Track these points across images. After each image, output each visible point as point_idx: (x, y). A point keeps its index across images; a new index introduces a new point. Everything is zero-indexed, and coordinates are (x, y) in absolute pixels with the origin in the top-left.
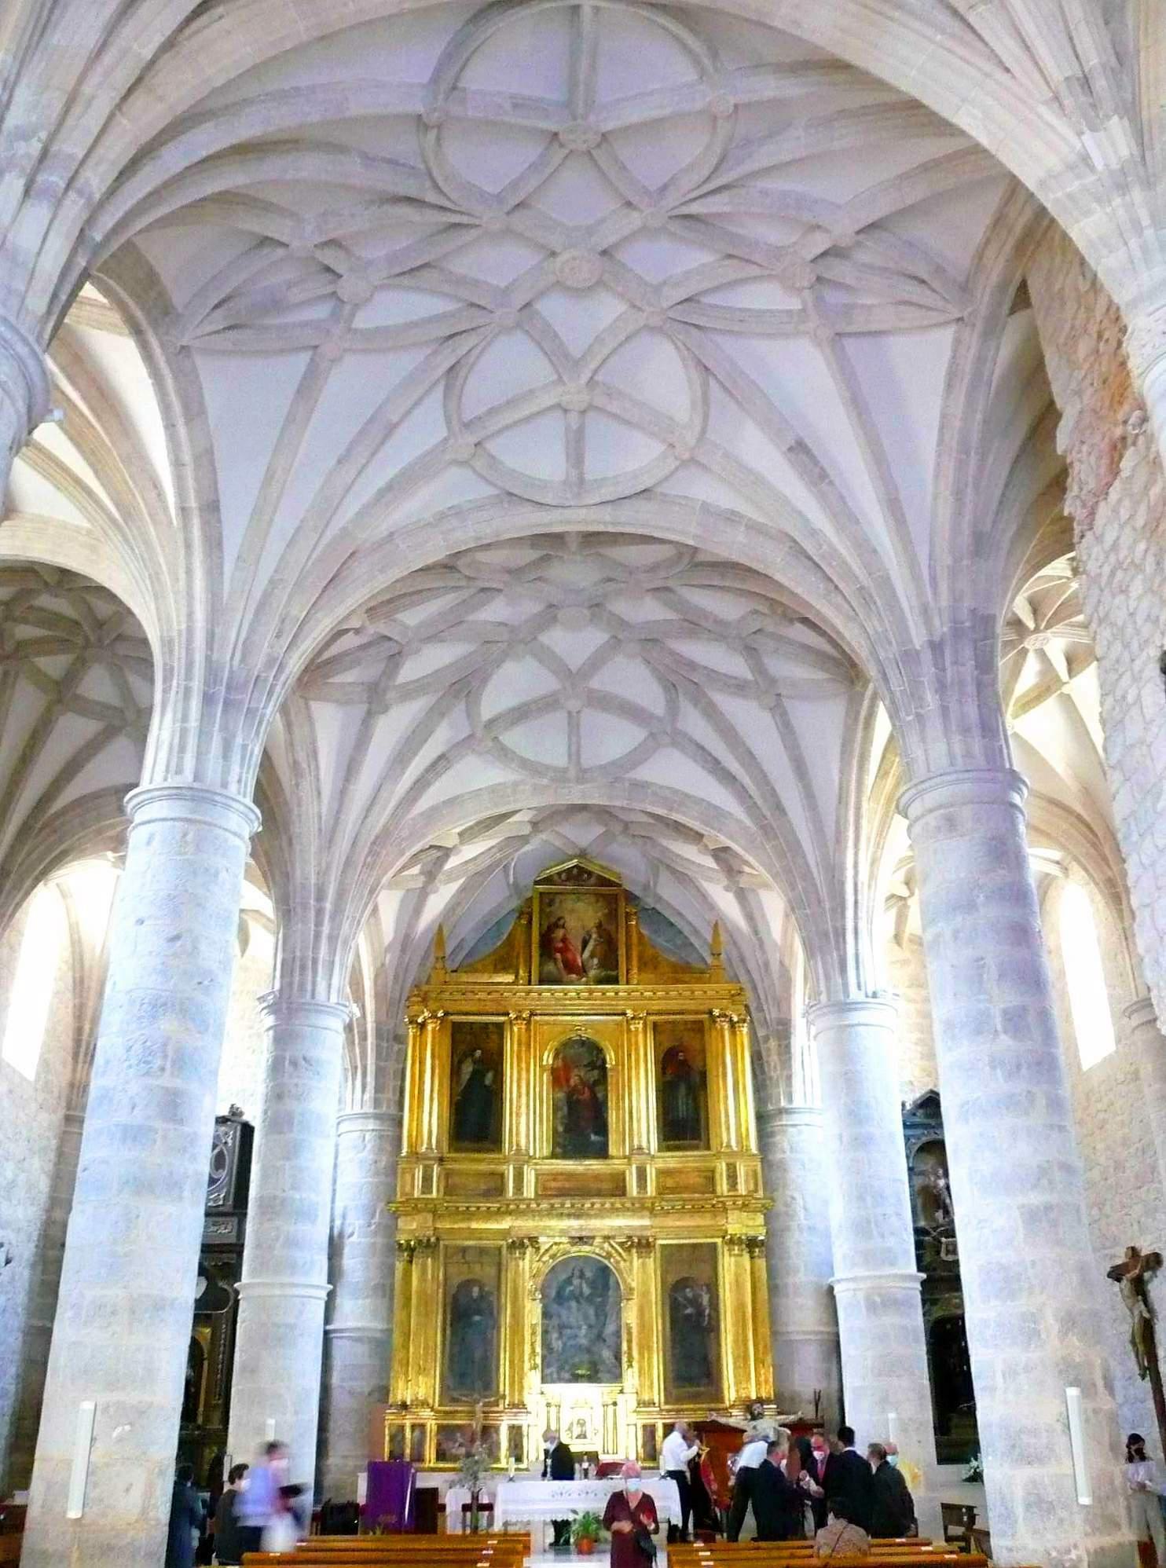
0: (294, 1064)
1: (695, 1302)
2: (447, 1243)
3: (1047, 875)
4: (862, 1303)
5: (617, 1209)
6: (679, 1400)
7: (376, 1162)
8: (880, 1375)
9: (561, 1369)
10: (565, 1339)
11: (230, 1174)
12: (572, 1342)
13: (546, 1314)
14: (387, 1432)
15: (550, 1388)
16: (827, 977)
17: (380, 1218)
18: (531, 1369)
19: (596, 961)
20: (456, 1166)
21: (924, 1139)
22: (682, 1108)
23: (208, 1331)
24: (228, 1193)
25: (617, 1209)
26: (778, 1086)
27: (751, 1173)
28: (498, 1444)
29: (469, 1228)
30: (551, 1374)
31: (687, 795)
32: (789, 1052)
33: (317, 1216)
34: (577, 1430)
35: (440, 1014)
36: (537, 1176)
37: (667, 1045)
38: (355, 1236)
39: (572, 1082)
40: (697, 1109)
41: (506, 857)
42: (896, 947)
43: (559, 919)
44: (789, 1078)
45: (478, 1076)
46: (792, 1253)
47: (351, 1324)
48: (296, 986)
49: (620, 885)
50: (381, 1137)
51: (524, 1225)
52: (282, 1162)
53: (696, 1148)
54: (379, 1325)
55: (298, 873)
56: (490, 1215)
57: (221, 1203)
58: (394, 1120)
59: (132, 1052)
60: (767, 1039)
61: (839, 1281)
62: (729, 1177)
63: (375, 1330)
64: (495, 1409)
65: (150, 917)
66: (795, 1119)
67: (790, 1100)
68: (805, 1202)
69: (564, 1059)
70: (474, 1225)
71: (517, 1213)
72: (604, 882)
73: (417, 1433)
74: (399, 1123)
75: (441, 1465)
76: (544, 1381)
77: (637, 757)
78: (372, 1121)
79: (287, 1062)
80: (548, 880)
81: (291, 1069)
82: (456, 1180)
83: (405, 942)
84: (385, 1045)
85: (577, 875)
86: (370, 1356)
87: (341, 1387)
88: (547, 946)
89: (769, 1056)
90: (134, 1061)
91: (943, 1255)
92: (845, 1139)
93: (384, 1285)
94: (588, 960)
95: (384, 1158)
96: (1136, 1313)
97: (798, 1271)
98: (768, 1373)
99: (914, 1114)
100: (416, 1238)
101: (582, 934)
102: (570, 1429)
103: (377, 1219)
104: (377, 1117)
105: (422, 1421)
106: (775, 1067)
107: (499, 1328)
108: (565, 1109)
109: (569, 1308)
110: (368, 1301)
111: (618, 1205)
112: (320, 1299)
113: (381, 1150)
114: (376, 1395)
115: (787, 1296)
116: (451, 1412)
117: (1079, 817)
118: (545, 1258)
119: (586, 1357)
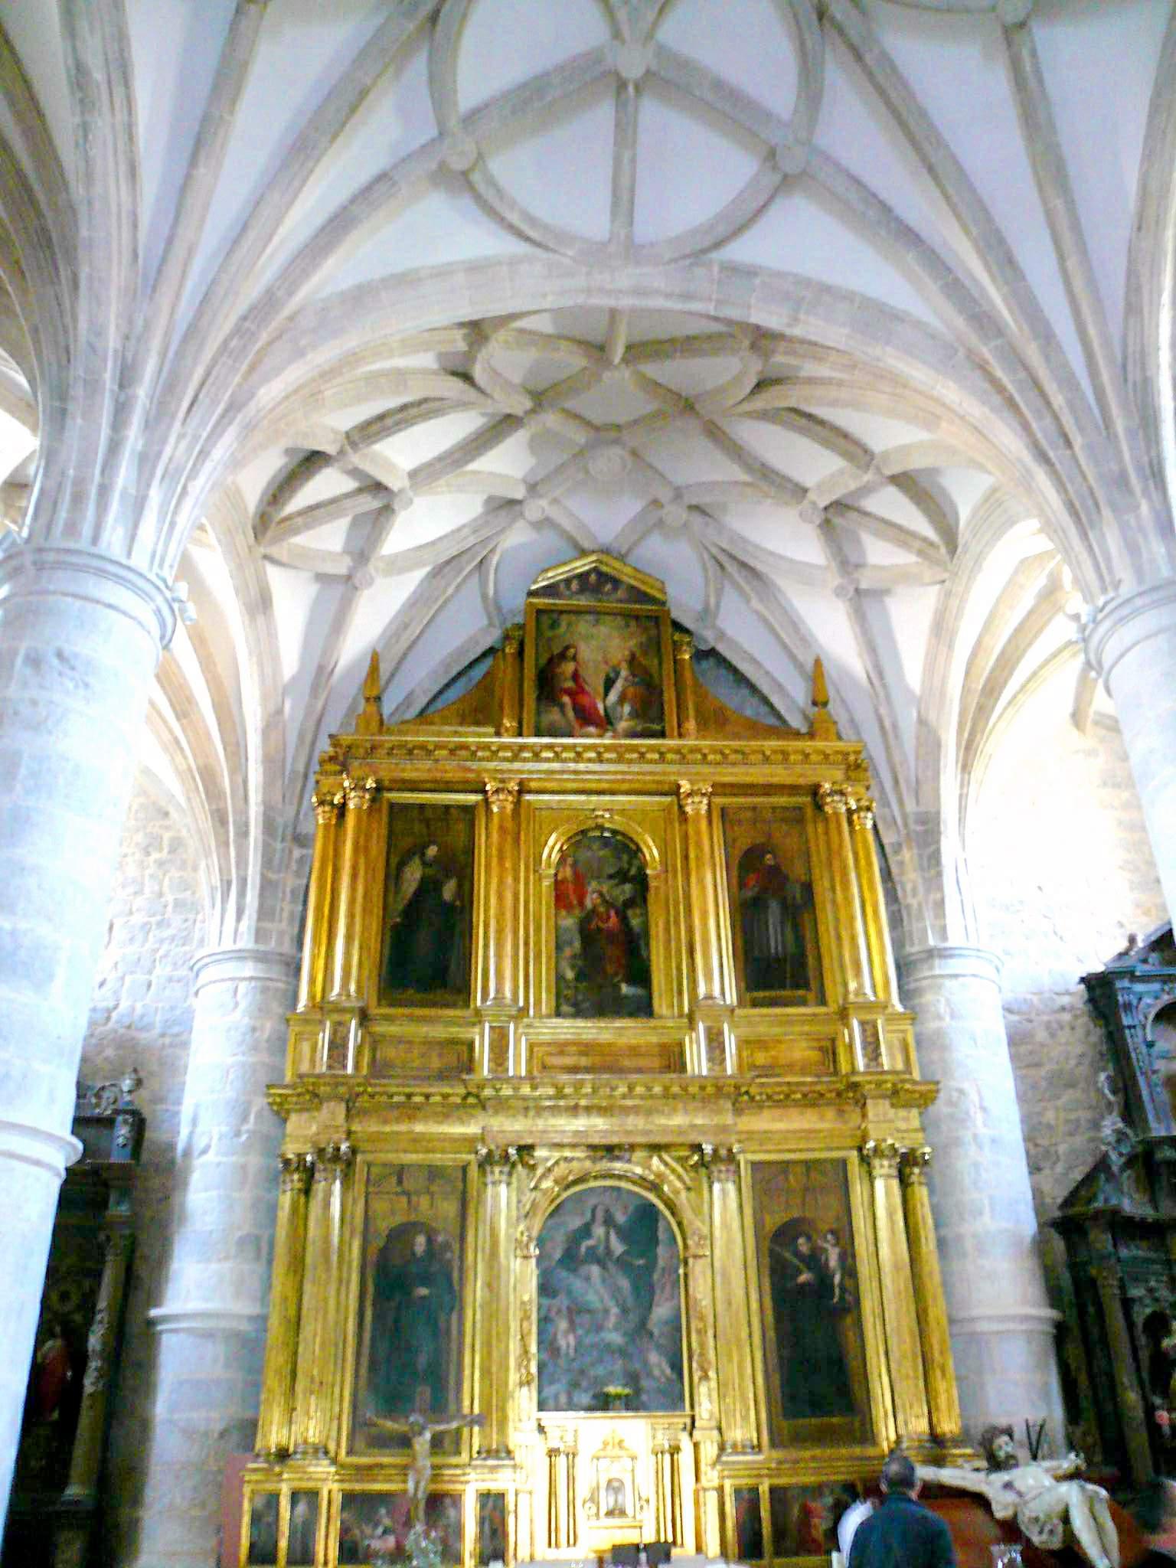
0: (35, 661)
1: (814, 1262)
2: (370, 1157)
5: (675, 1097)
6: (797, 1439)
7: (254, 1029)
9: (575, 1385)
10: (580, 1332)
12: (591, 1339)
13: (546, 1289)
14: (246, 1506)
15: (549, 1418)
17: (256, 1123)
18: (521, 1384)
20: (393, 1029)
22: (776, 937)
25: (675, 1097)
26: (920, 917)
27: (896, 1043)
28: (459, 1531)
29: (411, 1132)
30: (556, 1397)
31: (827, 289)
32: (938, 863)
33: (51, 977)
34: (606, 1501)
35: (370, 784)
36: (531, 1048)
37: (744, 843)
39: (589, 904)
40: (800, 939)
41: (484, 542)
42: (1075, 731)
43: (567, 648)
44: (940, 904)
45: (429, 887)
46: (967, 1181)
47: (193, 1305)
49: (663, 603)
50: (265, 990)
51: (510, 1127)
53: (803, 1003)
54: (248, 1308)
55: (83, 324)
56: (448, 1111)
58: (288, 964)
60: (898, 848)
62: (865, 1045)
63: (239, 1317)
64: (454, 1460)
68: (981, 1099)
69: (574, 865)
70: (419, 1128)
71: (501, 1105)
72: (639, 595)
73: (301, 1508)
74: (294, 968)
76: (541, 1407)
79: (19, 661)
80: (550, 590)
82: (389, 1052)
83: (321, 674)
84: (279, 846)
85: (596, 582)
86: (227, 1366)
87: (170, 1422)
88: (547, 687)
89: (902, 874)
93: (258, 1238)
95: (268, 1025)
97: (981, 1214)
99: (1145, 961)
100: (314, 1144)
101: (603, 670)
102: (594, 1499)
103: (250, 1125)
105: (311, 1485)
107: (462, 1309)
108: (577, 944)
109: (587, 1279)
110: (228, 1265)
111: (675, 1089)
112: (48, 1167)
113: (262, 1010)
114: (235, 1437)
115: (964, 1255)
116: (370, 1467)
118: (547, 1184)
119: (618, 1365)
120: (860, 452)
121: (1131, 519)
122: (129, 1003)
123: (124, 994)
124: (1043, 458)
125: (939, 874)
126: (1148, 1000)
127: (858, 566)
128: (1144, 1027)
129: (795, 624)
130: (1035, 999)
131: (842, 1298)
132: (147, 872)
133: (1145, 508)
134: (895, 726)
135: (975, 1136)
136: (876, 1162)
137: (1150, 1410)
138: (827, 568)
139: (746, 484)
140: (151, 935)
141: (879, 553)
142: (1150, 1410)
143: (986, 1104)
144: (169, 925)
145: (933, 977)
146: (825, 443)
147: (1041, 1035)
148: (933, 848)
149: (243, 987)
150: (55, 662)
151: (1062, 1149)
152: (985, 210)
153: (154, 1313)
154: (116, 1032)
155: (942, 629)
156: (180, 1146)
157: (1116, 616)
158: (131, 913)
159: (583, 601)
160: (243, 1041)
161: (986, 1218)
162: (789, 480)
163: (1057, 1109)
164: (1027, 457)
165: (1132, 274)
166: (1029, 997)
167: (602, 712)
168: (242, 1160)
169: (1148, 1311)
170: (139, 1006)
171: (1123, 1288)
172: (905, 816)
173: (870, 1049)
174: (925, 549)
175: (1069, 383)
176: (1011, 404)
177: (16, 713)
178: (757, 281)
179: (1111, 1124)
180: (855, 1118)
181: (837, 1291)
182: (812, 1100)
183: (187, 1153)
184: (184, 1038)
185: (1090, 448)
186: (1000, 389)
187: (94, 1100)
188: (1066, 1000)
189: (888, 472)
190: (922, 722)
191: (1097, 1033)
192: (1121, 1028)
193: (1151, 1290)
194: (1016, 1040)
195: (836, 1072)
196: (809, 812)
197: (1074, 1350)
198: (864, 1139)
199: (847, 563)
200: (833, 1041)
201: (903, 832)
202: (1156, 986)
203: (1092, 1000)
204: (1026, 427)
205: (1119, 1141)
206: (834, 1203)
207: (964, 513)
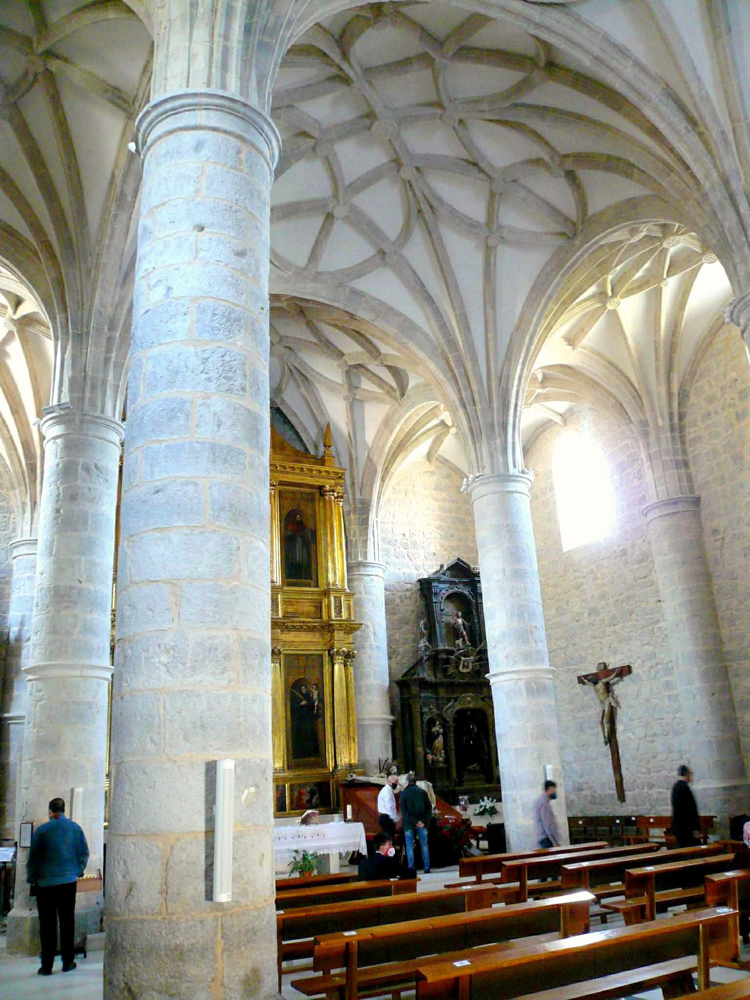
1: (308, 696)
3: (551, 420)
4: (523, 689)
8: (537, 739)
16: (492, 456)
21: (450, 591)
22: (299, 555)
31: (391, 309)
40: (309, 555)
42: (427, 462)
48: (87, 400)
52: (78, 557)
53: (309, 585)
59: (210, 364)
61: (494, 675)
65: (213, 225)
66: (370, 570)
67: (366, 557)
77: (361, 270)
79: (80, 468)
81: (84, 474)
90: (213, 374)
91: (461, 668)
92: (506, 573)
96: (607, 703)
98: (354, 747)
99: (444, 574)
106: (354, 533)
117: (627, 378)
121: (492, 442)
124: (464, 406)
125: (367, 528)
126: (444, 591)
127: (356, 388)
128: (441, 603)
129: (319, 404)
130: (397, 585)
133: (498, 441)
134: (357, 458)
136: (337, 657)
137: (426, 754)
138: (342, 385)
141: (366, 384)
142: (426, 754)
143: (376, 632)
145: (359, 574)
147: (398, 601)
148: (364, 516)
151: (400, 650)
152: (462, 302)
153: (6, 715)
155: (388, 423)
156: (12, 636)
157: (482, 481)
161: (372, 679)
162: (336, 348)
163: (400, 633)
164: (457, 402)
165: (510, 345)
166: (394, 583)
169: (428, 717)
171: (421, 709)
172: (354, 499)
173: (338, 609)
174: (390, 391)
175: (481, 384)
177: (83, 494)
178: (363, 299)
179: (423, 643)
180: (328, 636)
182: (311, 629)
183: (18, 639)
184: (7, 579)
185: (482, 410)
186: (452, 371)
188: (409, 586)
190: (368, 457)
191: (421, 603)
193: (430, 709)
194: (388, 602)
195: (321, 617)
196: (317, 496)
197: (398, 732)
198: (332, 648)
199: (353, 387)
200: (321, 603)
201: (352, 506)
202: (447, 586)
203: (421, 589)
204: (459, 390)
205: (426, 650)
206: (316, 672)
207: (412, 384)
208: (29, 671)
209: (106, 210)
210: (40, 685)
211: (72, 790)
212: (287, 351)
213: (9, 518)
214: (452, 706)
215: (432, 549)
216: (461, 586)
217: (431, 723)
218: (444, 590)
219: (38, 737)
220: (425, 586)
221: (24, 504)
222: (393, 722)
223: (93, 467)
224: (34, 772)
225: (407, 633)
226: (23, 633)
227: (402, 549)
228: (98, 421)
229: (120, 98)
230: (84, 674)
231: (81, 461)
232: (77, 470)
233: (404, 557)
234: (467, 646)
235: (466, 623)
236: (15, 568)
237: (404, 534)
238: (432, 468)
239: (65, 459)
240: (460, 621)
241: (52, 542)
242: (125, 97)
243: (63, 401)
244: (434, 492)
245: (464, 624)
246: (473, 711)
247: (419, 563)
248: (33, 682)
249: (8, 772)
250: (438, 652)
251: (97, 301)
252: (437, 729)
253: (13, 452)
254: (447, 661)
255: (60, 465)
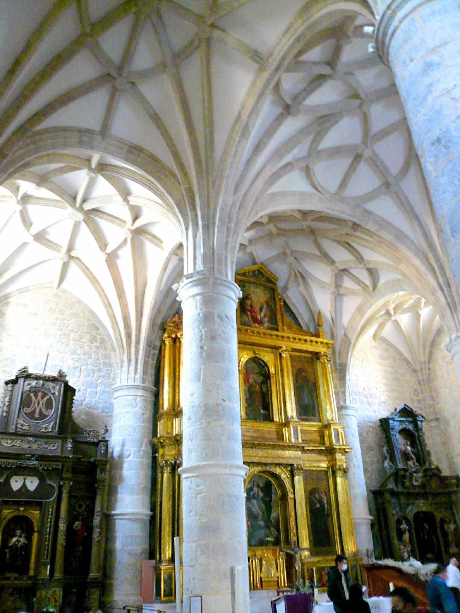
1: (320, 501)
7: (143, 414)
11: (56, 412)
19: (266, 319)
23: (37, 512)
24: (55, 424)
38: (131, 456)
47: (129, 510)
50: (146, 400)
53: (315, 421)
57: (50, 430)
63: (143, 514)
75: (173, 595)
77: (371, 196)
78: (141, 390)
79: (216, 316)
91: (414, 482)
94: (263, 318)
104: (144, 389)
110: (140, 496)
120: (359, 257)
122: (89, 399)
123: (87, 395)
131: (328, 512)
132: (93, 350)
135: (354, 465)
139: (317, 256)
140: (95, 374)
144: (102, 372)
145: (343, 415)
146: (350, 252)
149: (138, 399)
150: (226, 319)
153: (113, 512)
154: (85, 409)
155: (360, 310)
156: (116, 454)
158: (87, 365)
159: (253, 280)
160: (140, 418)
164: (436, 287)
167: (259, 318)
168: (142, 460)
170: (93, 400)
176: (433, 270)
177: (220, 335)
179: (387, 463)
181: (326, 510)
183: (121, 456)
184: (110, 413)
187: (87, 436)
188: (371, 424)
189: (368, 266)
190: (345, 335)
191: (381, 434)
192: (390, 434)
193: (397, 512)
194: (360, 435)
195: (324, 444)
197: (376, 528)
205: (390, 468)
206: (324, 483)
207: (382, 281)
208: (187, 470)
209: (230, 138)
210: (199, 481)
211: (232, 569)
212: (294, 261)
213: (111, 371)
214: (412, 510)
215: (382, 399)
216: (407, 423)
217: (399, 522)
218: (396, 426)
219: (201, 523)
220: (384, 423)
221: (122, 361)
222: (372, 521)
223: (224, 317)
224: (199, 553)
225: (374, 456)
226: (124, 451)
227: (364, 398)
228: (225, 283)
229: (258, 56)
230: (232, 472)
231: (216, 311)
232: (214, 317)
233: (366, 404)
234: (417, 466)
235: (413, 450)
236: (116, 406)
237: (364, 389)
238: (377, 344)
239: (204, 310)
240: (409, 448)
241: (200, 370)
242: (261, 56)
243: (198, 269)
244: (379, 360)
245: (412, 451)
246: (425, 513)
247: (375, 408)
248: (192, 479)
249: (115, 557)
250: (398, 470)
251: (220, 201)
252: (404, 526)
253: (115, 325)
254: (404, 477)
255: (201, 315)
